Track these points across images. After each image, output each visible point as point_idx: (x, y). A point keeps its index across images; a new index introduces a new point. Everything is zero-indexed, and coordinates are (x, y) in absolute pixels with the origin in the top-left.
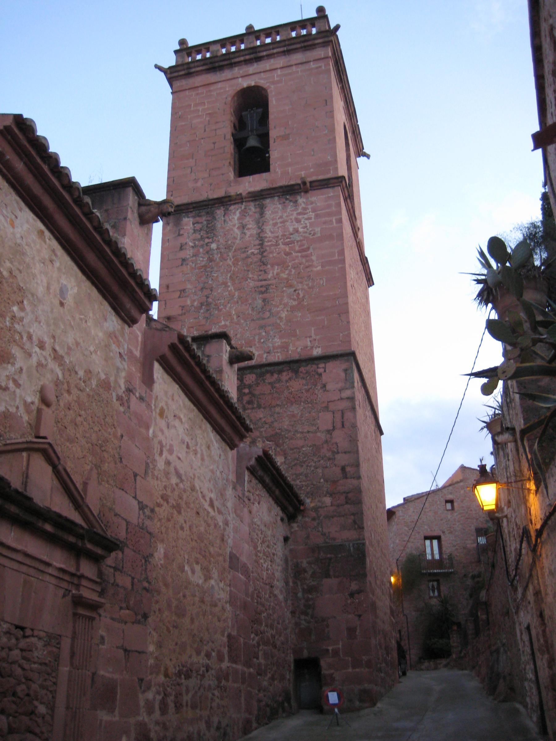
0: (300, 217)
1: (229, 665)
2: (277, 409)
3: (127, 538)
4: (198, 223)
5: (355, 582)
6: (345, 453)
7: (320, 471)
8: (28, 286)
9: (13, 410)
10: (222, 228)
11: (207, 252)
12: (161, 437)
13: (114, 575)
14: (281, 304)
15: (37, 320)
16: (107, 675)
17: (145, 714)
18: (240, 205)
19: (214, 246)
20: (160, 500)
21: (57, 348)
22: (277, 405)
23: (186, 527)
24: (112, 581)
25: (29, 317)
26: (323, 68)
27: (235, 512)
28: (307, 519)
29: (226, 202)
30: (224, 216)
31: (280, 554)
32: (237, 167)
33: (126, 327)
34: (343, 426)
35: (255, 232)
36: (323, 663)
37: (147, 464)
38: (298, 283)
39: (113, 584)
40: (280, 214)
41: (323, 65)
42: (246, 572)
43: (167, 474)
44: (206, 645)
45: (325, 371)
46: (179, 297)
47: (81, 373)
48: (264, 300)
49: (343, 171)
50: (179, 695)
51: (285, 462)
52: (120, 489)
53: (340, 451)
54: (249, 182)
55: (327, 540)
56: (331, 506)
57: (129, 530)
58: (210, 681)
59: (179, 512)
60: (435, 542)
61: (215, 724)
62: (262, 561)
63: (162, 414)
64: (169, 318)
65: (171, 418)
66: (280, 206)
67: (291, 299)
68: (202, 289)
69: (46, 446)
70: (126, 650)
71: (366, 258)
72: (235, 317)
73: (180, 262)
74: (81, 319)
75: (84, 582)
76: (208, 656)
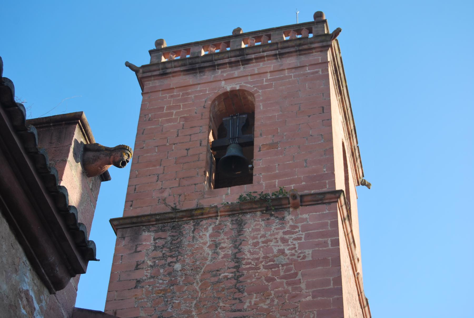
33: (46, 291)
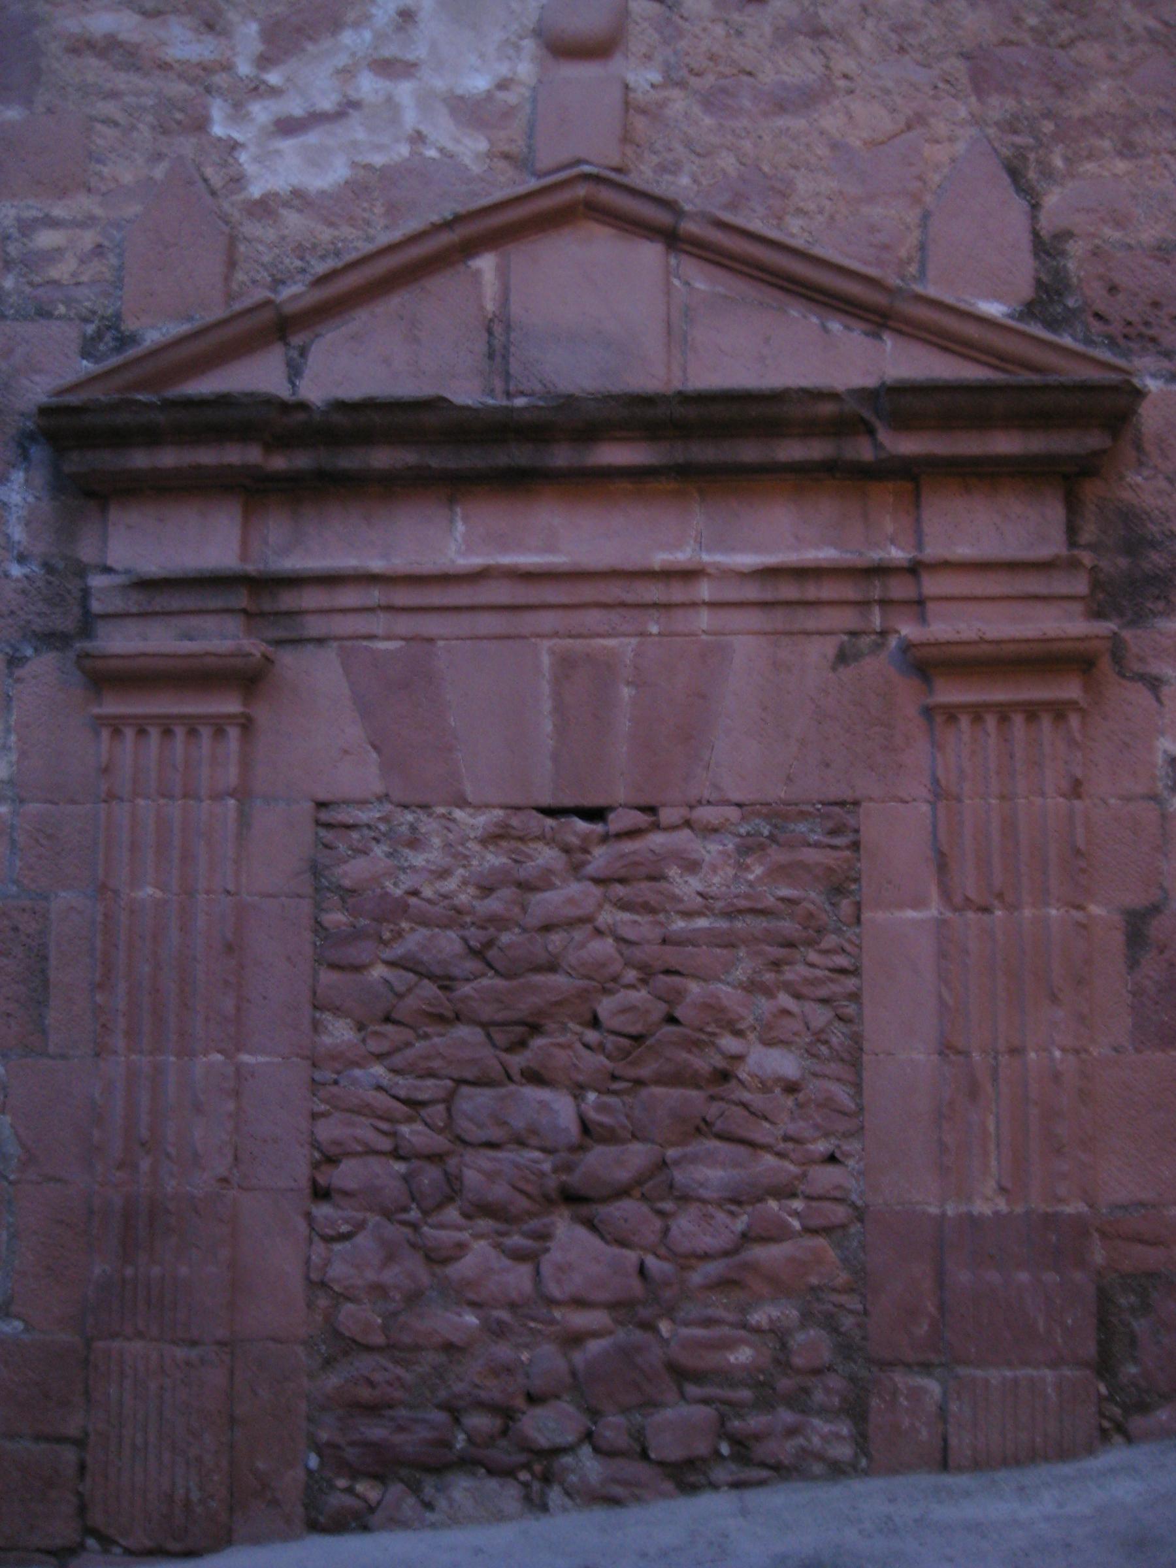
69: (582, 191)
75: (932, 585)
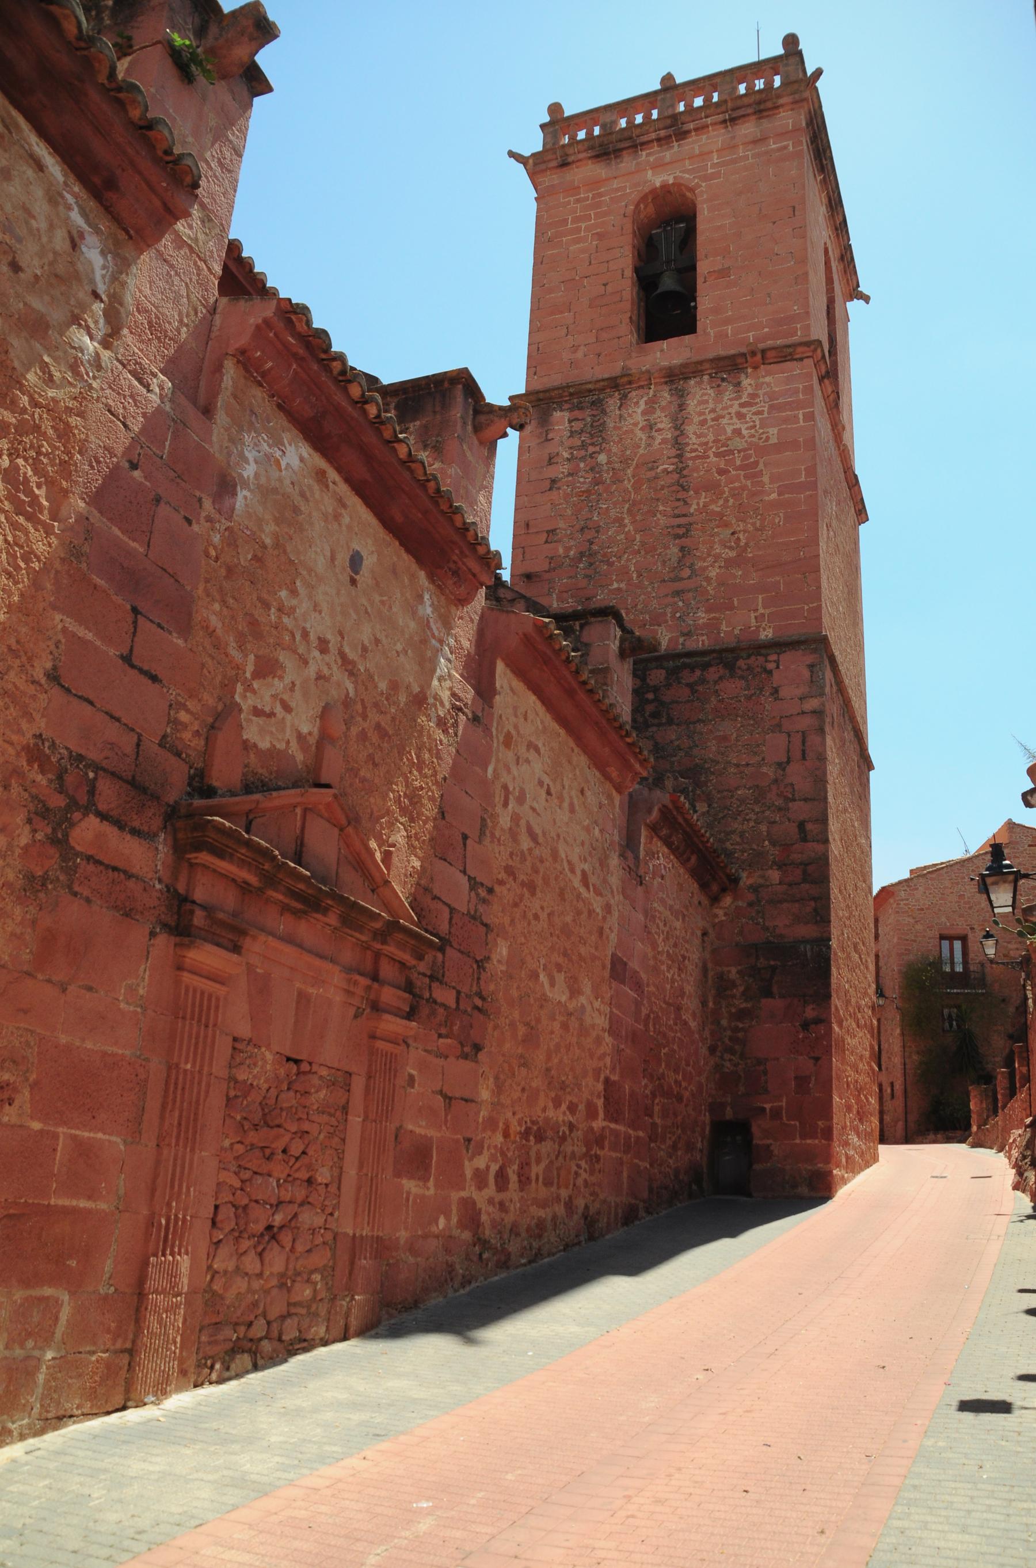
0: (744, 410)
1: (605, 1124)
2: (699, 727)
3: (450, 933)
4: (577, 419)
5: (811, 1006)
6: (806, 800)
7: (763, 828)
8: (302, 558)
9: (281, 746)
10: (616, 428)
11: (592, 469)
12: (505, 778)
13: (430, 987)
14: (709, 555)
15: (316, 608)
16: (418, 1130)
17: (473, 1188)
18: (646, 391)
19: (602, 458)
20: (502, 875)
21: (347, 650)
22: (699, 721)
23: (543, 916)
24: (427, 995)
25: (304, 605)
26: (791, 148)
27: (624, 893)
28: (740, 903)
29: (624, 385)
30: (620, 408)
31: (695, 956)
32: (642, 324)
34: (804, 758)
35: (669, 436)
36: (754, 1129)
37: (483, 820)
38: (738, 521)
39: (427, 1000)
40: (711, 406)
41: (791, 143)
42: (638, 986)
43: (514, 835)
44: (569, 1093)
45: (778, 667)
46: (546, 542)
47: (383, 686)
48: (682, 549)
49: (819, 332)
50: (524, 1166)
51: (708, 812)
52: (441, 858)
53: (797, 797)
54: (662, 351)
55: (771, 939)
56: (780, 883)
57: (454, 922)
58: (575, 1146)
59: (533, 894)
60: (958, 945)
61: (580, 1210)
62: (664, 968)
63: (508, 742)
64: (529, 577)
65: (522, 750)
66: (711, 392)
67: (726, 547)
68: (582, 529)
70: (446, 1097)
71: (856, 477)
72: (635, 576)
73: (547, 484)
74: (383, 602)
76: (572, 1108)
